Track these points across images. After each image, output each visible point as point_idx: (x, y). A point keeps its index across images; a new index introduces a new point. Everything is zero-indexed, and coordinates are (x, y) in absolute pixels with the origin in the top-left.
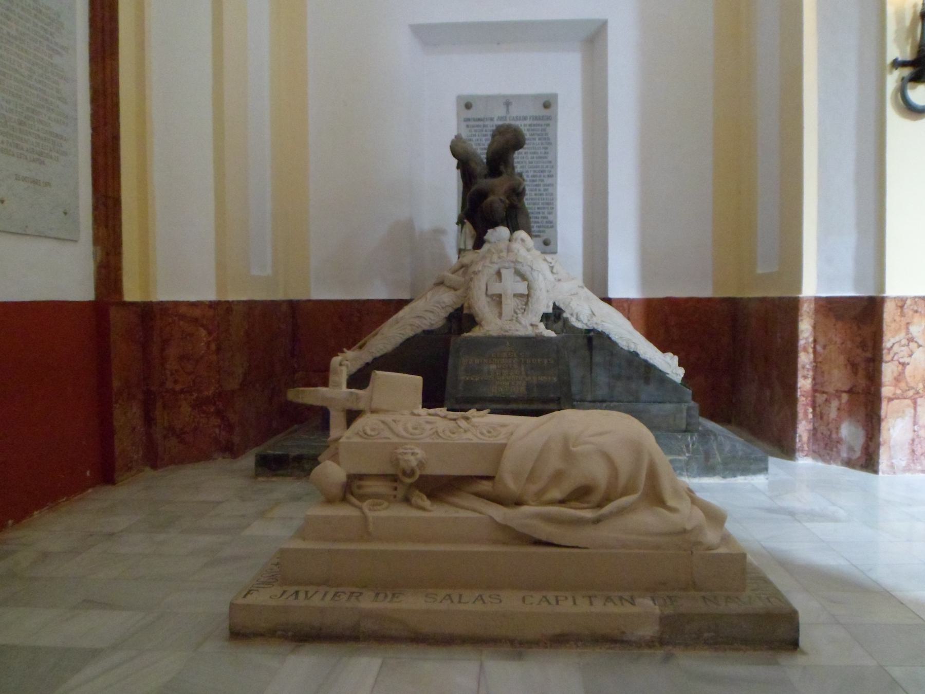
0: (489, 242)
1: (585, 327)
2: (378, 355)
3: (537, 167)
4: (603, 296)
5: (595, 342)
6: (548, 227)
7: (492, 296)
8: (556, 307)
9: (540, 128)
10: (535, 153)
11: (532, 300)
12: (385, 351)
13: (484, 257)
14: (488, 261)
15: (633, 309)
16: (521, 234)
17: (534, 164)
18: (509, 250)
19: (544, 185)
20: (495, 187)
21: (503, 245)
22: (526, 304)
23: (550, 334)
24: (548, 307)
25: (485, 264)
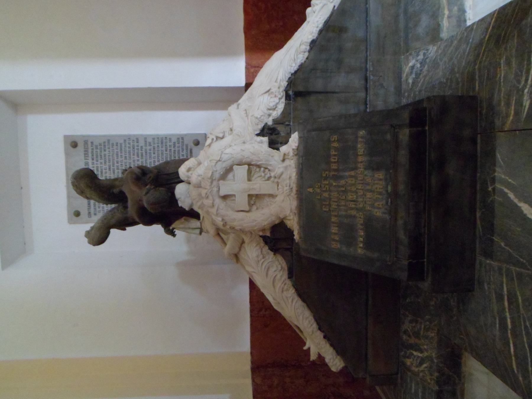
0: (192, 204)
1: (283, 100)
2: (315, 325)
3: (129, 152)
4: (244, 89)
5: (301, 88)
6: (183, 142)
7: (250, 205)
8: (262, 133)
9: (95, 151)
10: (117, 155)
11: (254, 159)
12: (311, 318)
13: (208, 213)
14: (210, 210)
15: (254, 63)
16: (182, 171)
17: (127, 155)
18: (198, 186)
19: (146, 145)
20: (139, 194)
21: (194, 193)
22: (259, 166)
23: (294, 138)
24: (261, 142)
25: (215, 212)
